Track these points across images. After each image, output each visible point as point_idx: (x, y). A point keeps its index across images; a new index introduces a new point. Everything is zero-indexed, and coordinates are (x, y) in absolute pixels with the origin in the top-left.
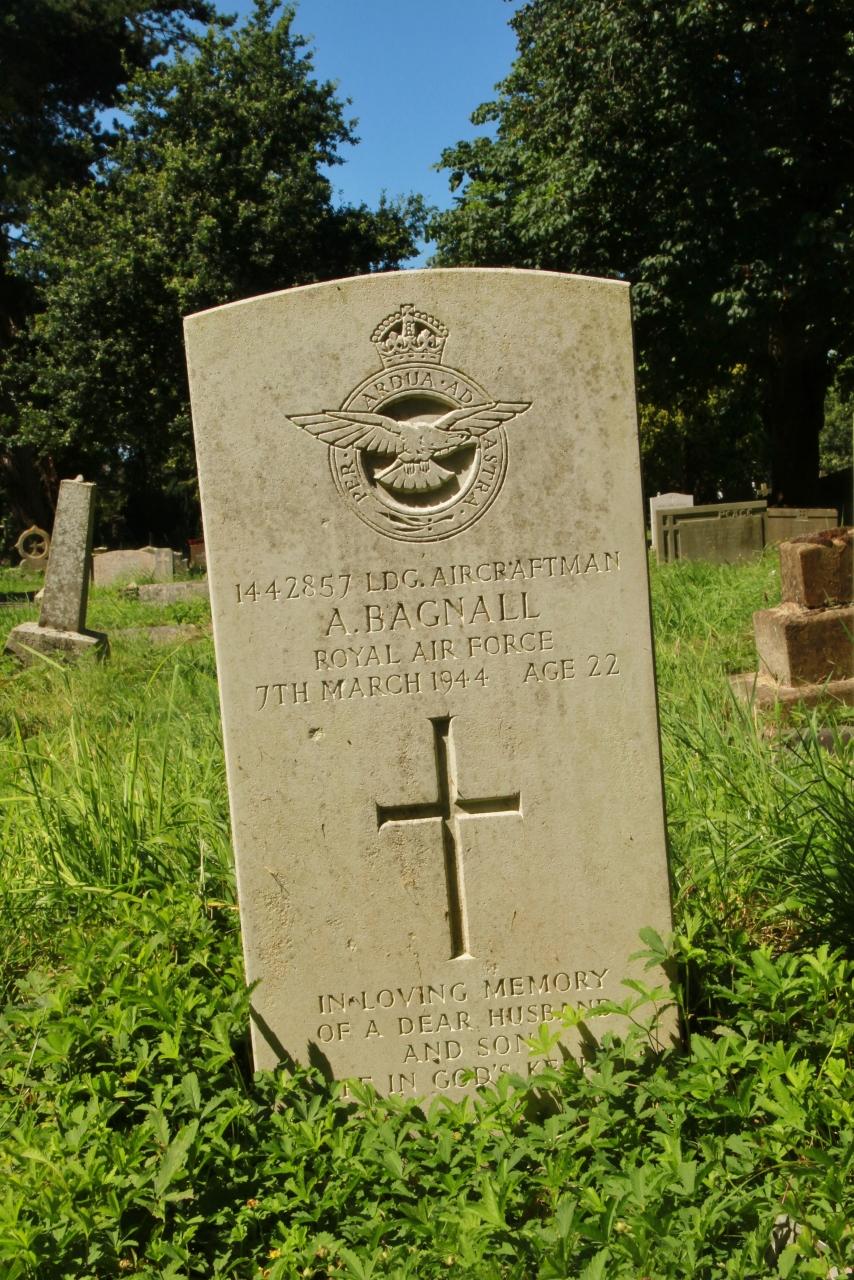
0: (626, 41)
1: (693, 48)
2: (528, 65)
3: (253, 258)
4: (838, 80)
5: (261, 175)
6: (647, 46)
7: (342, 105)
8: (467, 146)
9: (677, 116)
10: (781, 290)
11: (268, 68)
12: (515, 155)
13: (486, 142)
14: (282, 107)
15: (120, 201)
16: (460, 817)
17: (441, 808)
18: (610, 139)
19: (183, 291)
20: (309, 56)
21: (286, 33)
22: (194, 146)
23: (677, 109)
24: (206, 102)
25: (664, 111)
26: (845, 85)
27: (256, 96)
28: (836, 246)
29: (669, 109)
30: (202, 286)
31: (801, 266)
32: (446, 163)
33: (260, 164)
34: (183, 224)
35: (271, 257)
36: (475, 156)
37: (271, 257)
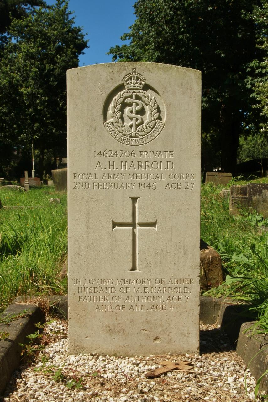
0: (168, 11)
1: (190, 14)
2: (141, 22)
3: (50, 83)
4: (240, 29)
5: (55, 56)
6: (175, 13)
7: (84, 35)
8: (118, 47)
9: (186, 37)
10: (220, 98)
11: (59, 21)
12: (134, 50)
13: (125, 46)
14: (62, 33)
15: (6, 62)
16: (138, 228)
17: (133, 225)
18: (164, 45)
19: (25, 92)
20: (73, 18)
21: (65, 10)
22: (32, 45)
23: (186, 35)
24: (37, 30)
25: (181, 36)
26: (243, 30)
27: (54, 30)
28: (239, 84)
29: (183, 36)
30: (32, 91)
31: (227, 91)
32: (111, 52)
33: (54, 52)
34: (26, 70)
35: (56, 83)
36: (121, 50)
37: (56, 83)
